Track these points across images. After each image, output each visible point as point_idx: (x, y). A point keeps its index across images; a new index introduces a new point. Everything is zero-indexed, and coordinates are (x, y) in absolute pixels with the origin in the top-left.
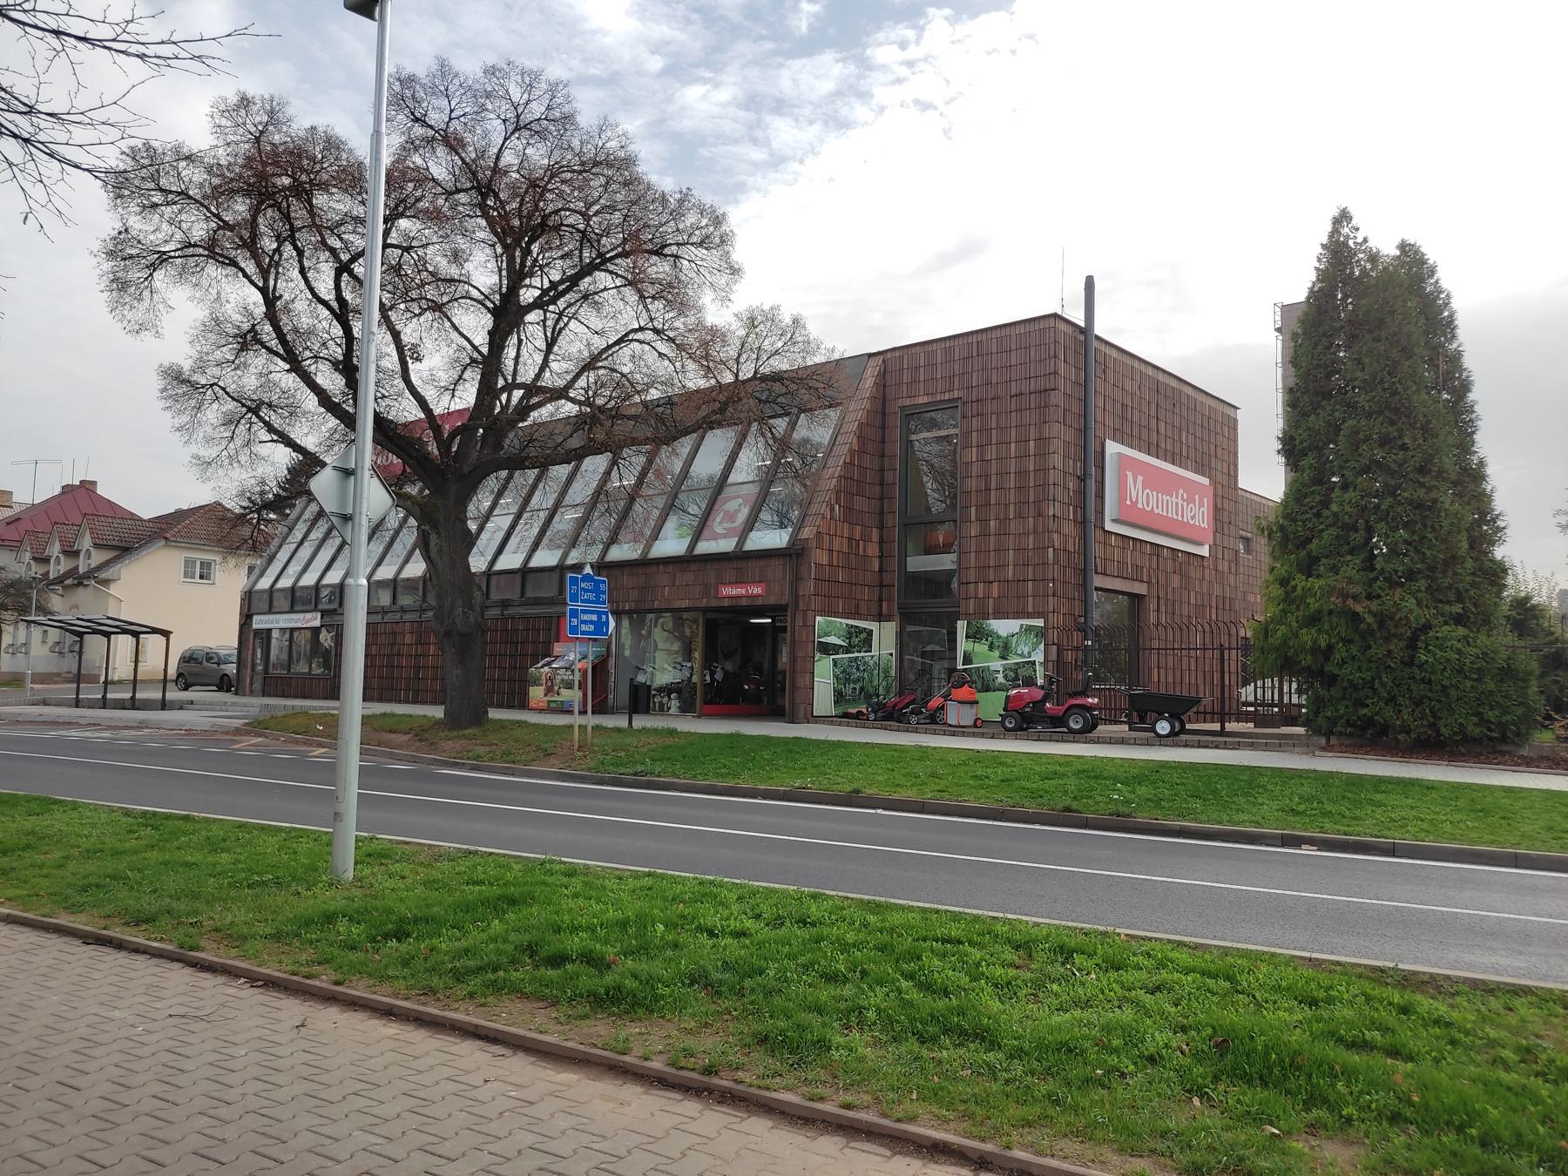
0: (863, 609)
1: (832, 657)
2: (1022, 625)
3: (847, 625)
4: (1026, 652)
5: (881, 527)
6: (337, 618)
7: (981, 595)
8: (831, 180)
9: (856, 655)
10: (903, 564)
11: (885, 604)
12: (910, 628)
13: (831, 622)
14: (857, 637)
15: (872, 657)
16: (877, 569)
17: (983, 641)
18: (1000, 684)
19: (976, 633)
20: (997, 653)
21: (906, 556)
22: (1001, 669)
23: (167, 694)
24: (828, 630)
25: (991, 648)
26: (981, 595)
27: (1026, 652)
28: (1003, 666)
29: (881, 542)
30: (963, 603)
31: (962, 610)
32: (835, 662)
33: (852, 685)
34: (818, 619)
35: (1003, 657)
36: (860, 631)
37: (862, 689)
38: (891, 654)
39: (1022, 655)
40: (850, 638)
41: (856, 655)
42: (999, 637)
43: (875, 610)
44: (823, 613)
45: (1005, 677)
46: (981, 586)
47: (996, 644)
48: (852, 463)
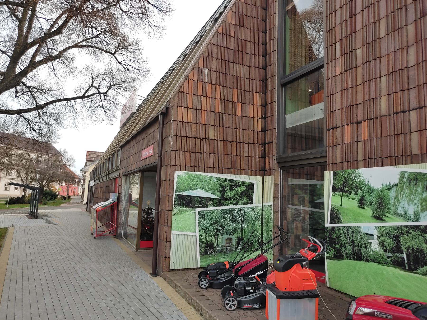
0: (242, 164)
1: (197, 210)
2: (402, 175)
3: (219, 179)
4: (411, 212)
5: (264, 92)
6: (350, 168)
7: (348, 139)
8: (371, 177)
9: (231, 207)
10: (282, 120)
11: (267, 159)
12: (293, 182)
13: (197, 177)
14: (232, 189)
15: (253, 209)
16: (260, 129)
17: (352, 195)
18: (375, 253)
19: (344, 185)
20: (369, 211)
21: (285, 114)
22: (375, 233)
23: (38, 211)
24: (191, 183)
25: (362, 203)
26: (348, 139)
27: (411, 212)
28: (379, 229)
29: (264, 105)
30: (329, 152)
31: (329, 160)
32: (202, 216)
33: (226, 236)
34: (177, 173)
35: (378, 218)
36: (235, 185)
37: (240, 239)
38: (271, 206)
39: (405, 217)
40: (223, 191)
41: (231, 207)
42: (371, 190)
43: (257, 163)
44: (185, 167)
45: (382, 244)
46: (348, 129)
47: (368, 199)
48: (226, 34)
